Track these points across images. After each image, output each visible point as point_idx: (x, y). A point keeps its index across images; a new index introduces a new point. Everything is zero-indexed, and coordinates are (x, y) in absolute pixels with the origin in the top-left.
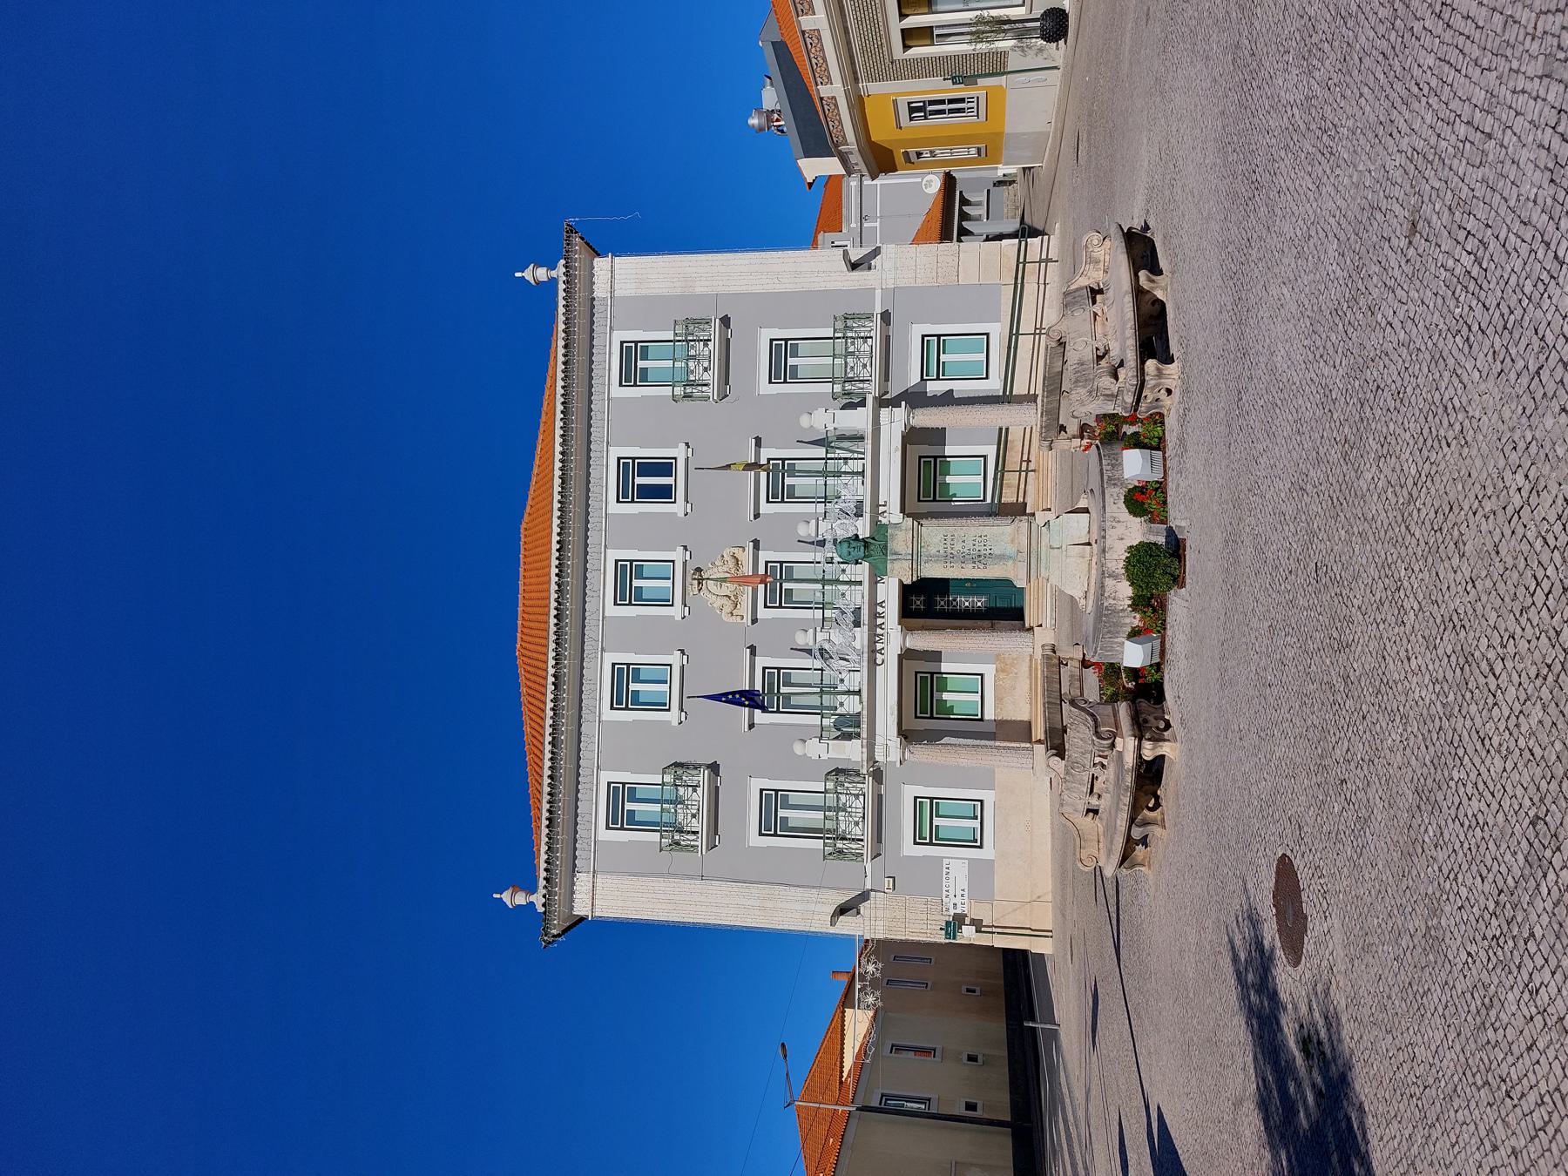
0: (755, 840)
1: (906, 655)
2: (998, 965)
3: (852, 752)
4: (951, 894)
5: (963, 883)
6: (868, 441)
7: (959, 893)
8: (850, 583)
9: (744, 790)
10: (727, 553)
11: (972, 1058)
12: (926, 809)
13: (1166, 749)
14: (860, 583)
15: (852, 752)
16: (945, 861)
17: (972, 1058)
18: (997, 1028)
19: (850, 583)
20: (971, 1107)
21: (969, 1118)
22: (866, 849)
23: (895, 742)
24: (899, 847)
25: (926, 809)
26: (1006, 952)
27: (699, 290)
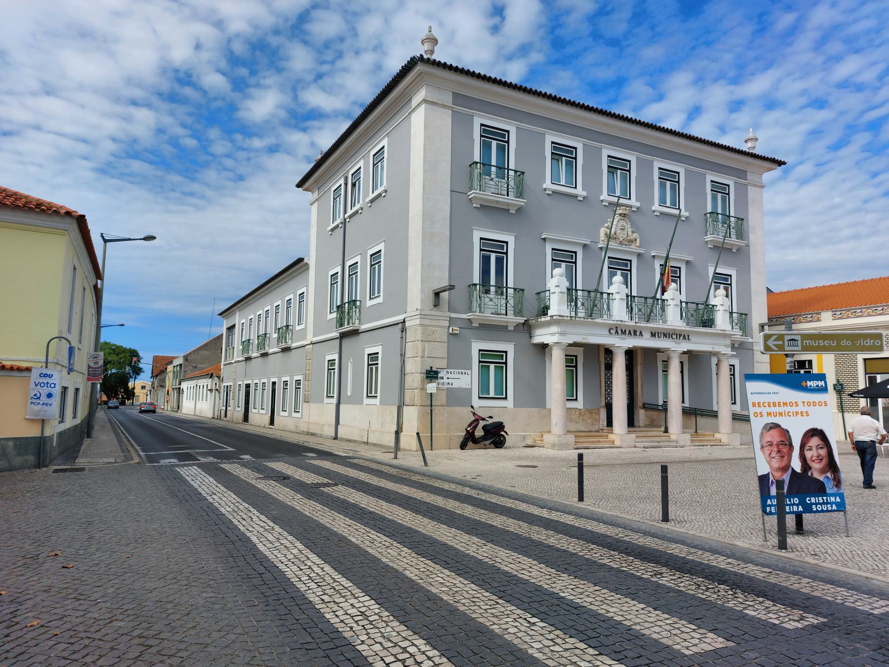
0: (477, 235)
1: (609, 352)
4: (449, 376)
5: (456, 384)
7: (450, 381)
9: (731, 179)
16: (469, 372)
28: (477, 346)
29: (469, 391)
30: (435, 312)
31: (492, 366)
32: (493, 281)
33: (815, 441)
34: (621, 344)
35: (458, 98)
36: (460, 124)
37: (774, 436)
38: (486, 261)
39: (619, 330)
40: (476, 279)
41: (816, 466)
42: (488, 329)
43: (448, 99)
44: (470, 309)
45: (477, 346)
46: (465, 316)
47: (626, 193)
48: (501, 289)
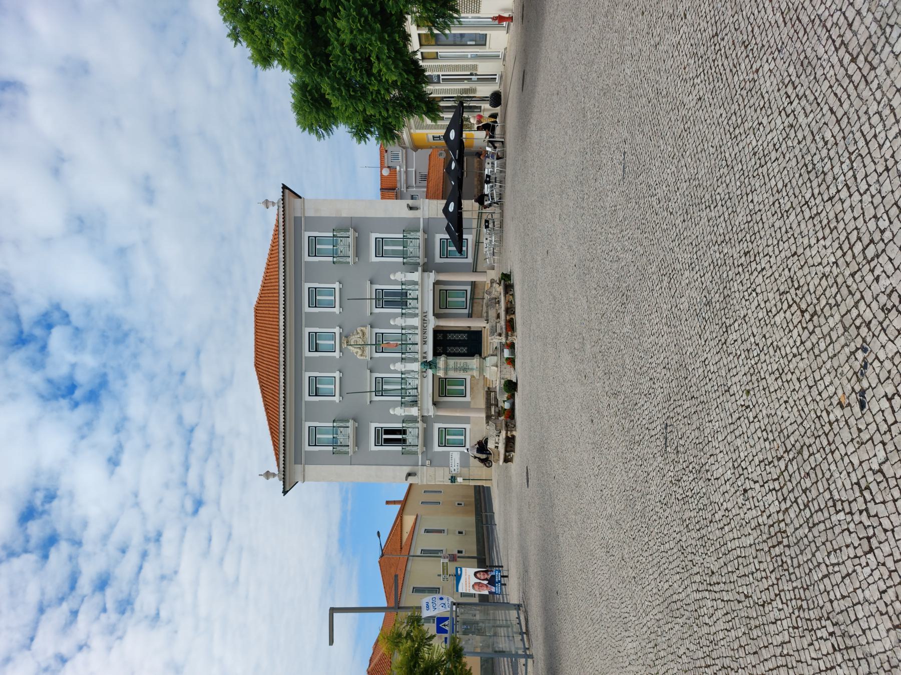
0: (374, 448)
1: (436, 332)
2: (472, 492)
3: (414, 411)
5: (458, 461)
6: (419, 331)
8: (413, 344)
9: (368, 428)
10: (359, 329)
11: (460, 533)
12: (443, 432)
13: (514, 433)
14: (427, 531)
15: (414, 411)
17: (460, 533)
18: (472, 519)
19: (413, 344)
20: (459, 552)
21: (43, 593)
22: (419, 450)
23: (431, 407)
24: (432, 447)
25: (443, 432)
26: (475, 486)
27: (344, 215)
28: (437, 448)
29: (462, 453)
30: (419, 474)
31: (447, 437)
32: (400, 437)
33: (478, 575)
34: (432, 322)
35: (298, 461)
36: (313, 459)
37: (477, 587)
38: (387, 441)
39: (424, 321)
40: (400, 448)
41: (486, 576)
42: (427, 442)
43: (299, 467)
44: (416, 453)
45: (437, 448)
46: (420, 456)
47: (332, 292)
48: (403, 432)
